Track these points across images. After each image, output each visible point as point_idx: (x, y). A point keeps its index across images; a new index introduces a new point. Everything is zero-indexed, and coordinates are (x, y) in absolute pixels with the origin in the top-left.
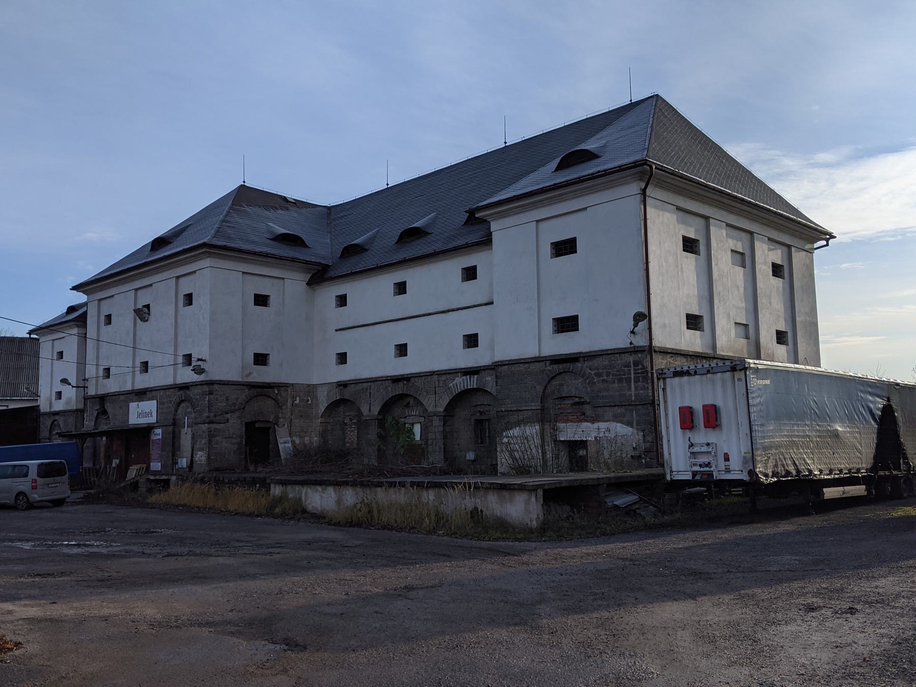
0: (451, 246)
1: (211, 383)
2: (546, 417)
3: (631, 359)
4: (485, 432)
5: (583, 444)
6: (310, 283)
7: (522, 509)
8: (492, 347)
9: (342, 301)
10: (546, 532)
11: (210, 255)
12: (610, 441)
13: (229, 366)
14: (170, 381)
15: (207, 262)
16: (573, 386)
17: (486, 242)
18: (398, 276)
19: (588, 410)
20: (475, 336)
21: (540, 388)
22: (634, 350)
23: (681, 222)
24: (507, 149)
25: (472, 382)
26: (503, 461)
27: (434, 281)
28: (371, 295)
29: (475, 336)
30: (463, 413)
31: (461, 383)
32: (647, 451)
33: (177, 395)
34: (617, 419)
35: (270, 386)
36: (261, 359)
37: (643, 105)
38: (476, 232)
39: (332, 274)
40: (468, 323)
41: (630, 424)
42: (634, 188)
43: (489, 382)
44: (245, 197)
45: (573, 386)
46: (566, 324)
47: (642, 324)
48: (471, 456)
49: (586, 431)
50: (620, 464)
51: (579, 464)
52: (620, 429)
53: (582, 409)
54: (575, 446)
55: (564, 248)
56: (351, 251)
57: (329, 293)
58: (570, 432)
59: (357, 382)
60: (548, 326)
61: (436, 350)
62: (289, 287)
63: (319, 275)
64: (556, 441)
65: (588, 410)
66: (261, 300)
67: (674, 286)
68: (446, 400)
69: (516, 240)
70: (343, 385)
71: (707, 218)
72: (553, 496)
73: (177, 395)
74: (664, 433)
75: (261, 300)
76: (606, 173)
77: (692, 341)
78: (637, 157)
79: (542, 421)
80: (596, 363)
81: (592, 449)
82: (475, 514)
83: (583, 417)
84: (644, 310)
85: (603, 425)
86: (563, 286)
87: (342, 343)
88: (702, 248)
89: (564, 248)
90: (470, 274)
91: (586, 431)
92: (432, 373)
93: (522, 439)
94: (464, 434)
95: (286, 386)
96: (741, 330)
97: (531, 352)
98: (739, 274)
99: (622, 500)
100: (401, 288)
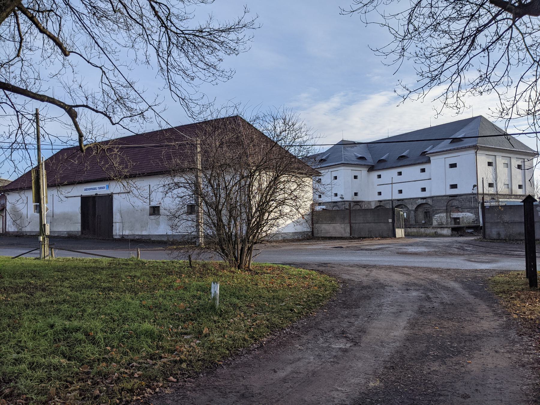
0: (417, 162)
1: (344, 201)
2: (447, 211)
3: (472, 196)
4: (428, 215)
5: (459, 218)
6: (368, 171)
7: (446, 232)
8: (431, 191)
9: (379, 176)
10: (452, 236)
11: (343, 166)
12: (466, 218)
13: (349, 197)
14: (330, 201)
15: (343, 168)
16: (455, 203)
17: (429, 161)
18: (399, 170)
19: (460, 209)
20: (425, 188)
21: (446, 204)
22: (473, 194)
23: (488, 158)
24: (431, 128)
25: (424, 201)
26: (435, 223)
27: (411, 172)
28: (389, 175)
29: (425, 188)
30: (420, 210)
31: (420, 202)
32: (476, 220)
33: (332, 205)
34: (468, 212)
35: (359, 202)
36: (356, 194)
37: (476, 119)
38: (424, 159)
39: (375, 169)
40: (423, 184)
41: (472, 213)
42: (473, 151)
43: (430, 201)
44: (344, 144)
45: (455, 203)
46: (454, 186)
47: (476, 188)
48: (423, 222)
49: (460, 215)
50: (469, 223)
51: (459, 223)
52: (469, 214)
53: (458, 209)
54: (456, 219)
55: (453, 166)
56: (380, 161)
57: (375, 174)
58: (455, 215)
59: (385, 201)
60: (449, 187)
61: (412, 192)
62: (363, 173)
63: (371, 169)
64: (450, 218)
65: (460, 209)
66: (356, 177)
67: (485, 173)
68: (415, 206)
69: (438, 164)
70: (381, 201)
71: (495, 156)
72: (453, 229)
73: (332, 205)
74: (305, 243)
75: (356, 177)
76: (465, 148)
77: (492, 191)
78: (474, 144)
79: (447, 212)
80: (462, 197)
81: (461, 220)
82: (435, 232)
83: (459, 211)
84: (476, 184)
85: (464, 213)
86: (454, 176)
87: (380, 189)
88: (494, 164)
89: (453, 166)
90: (423, 170)
91: (460, 215)
92: (411, 199)
93: (439, 217)
94: (421, 216)
95: (363, 201)
96: (506, 186)
97: (444, 194)
98: (506, 170)
99: (470, 231)
100: (400, 174)
